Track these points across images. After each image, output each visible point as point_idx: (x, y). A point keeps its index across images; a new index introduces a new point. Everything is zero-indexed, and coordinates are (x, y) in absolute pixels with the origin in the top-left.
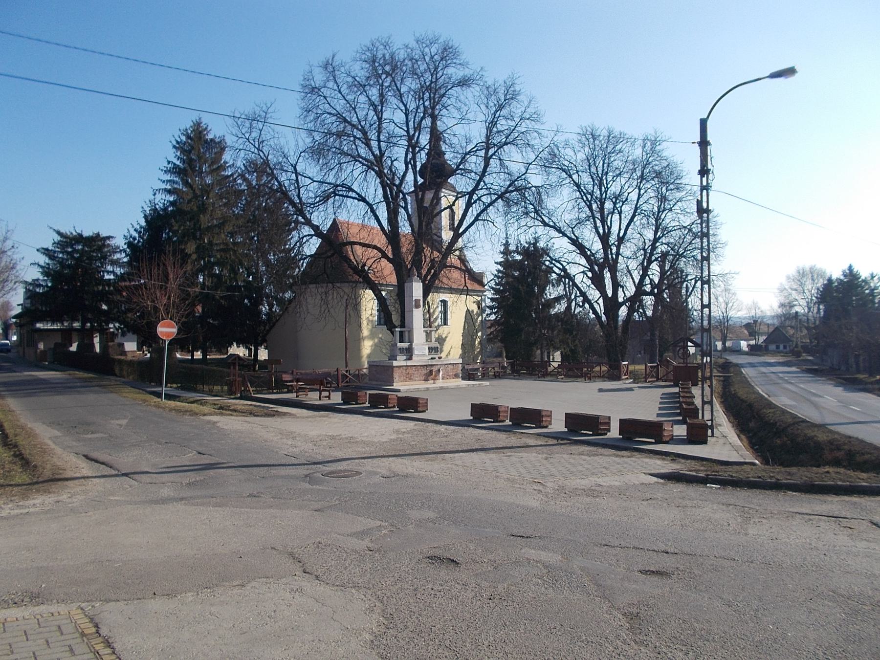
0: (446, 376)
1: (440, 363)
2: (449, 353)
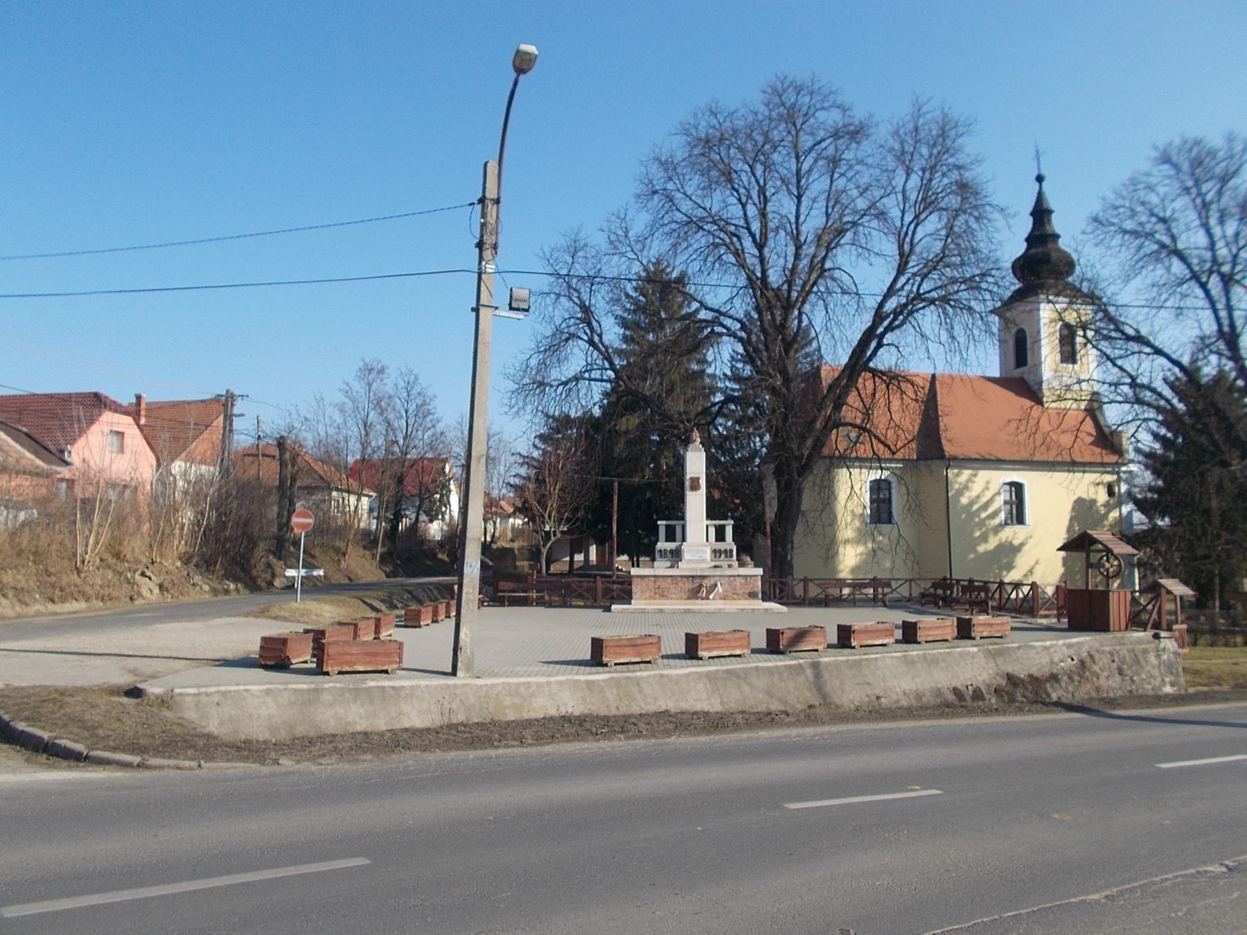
0: (730, 594)
1: (718, 573)
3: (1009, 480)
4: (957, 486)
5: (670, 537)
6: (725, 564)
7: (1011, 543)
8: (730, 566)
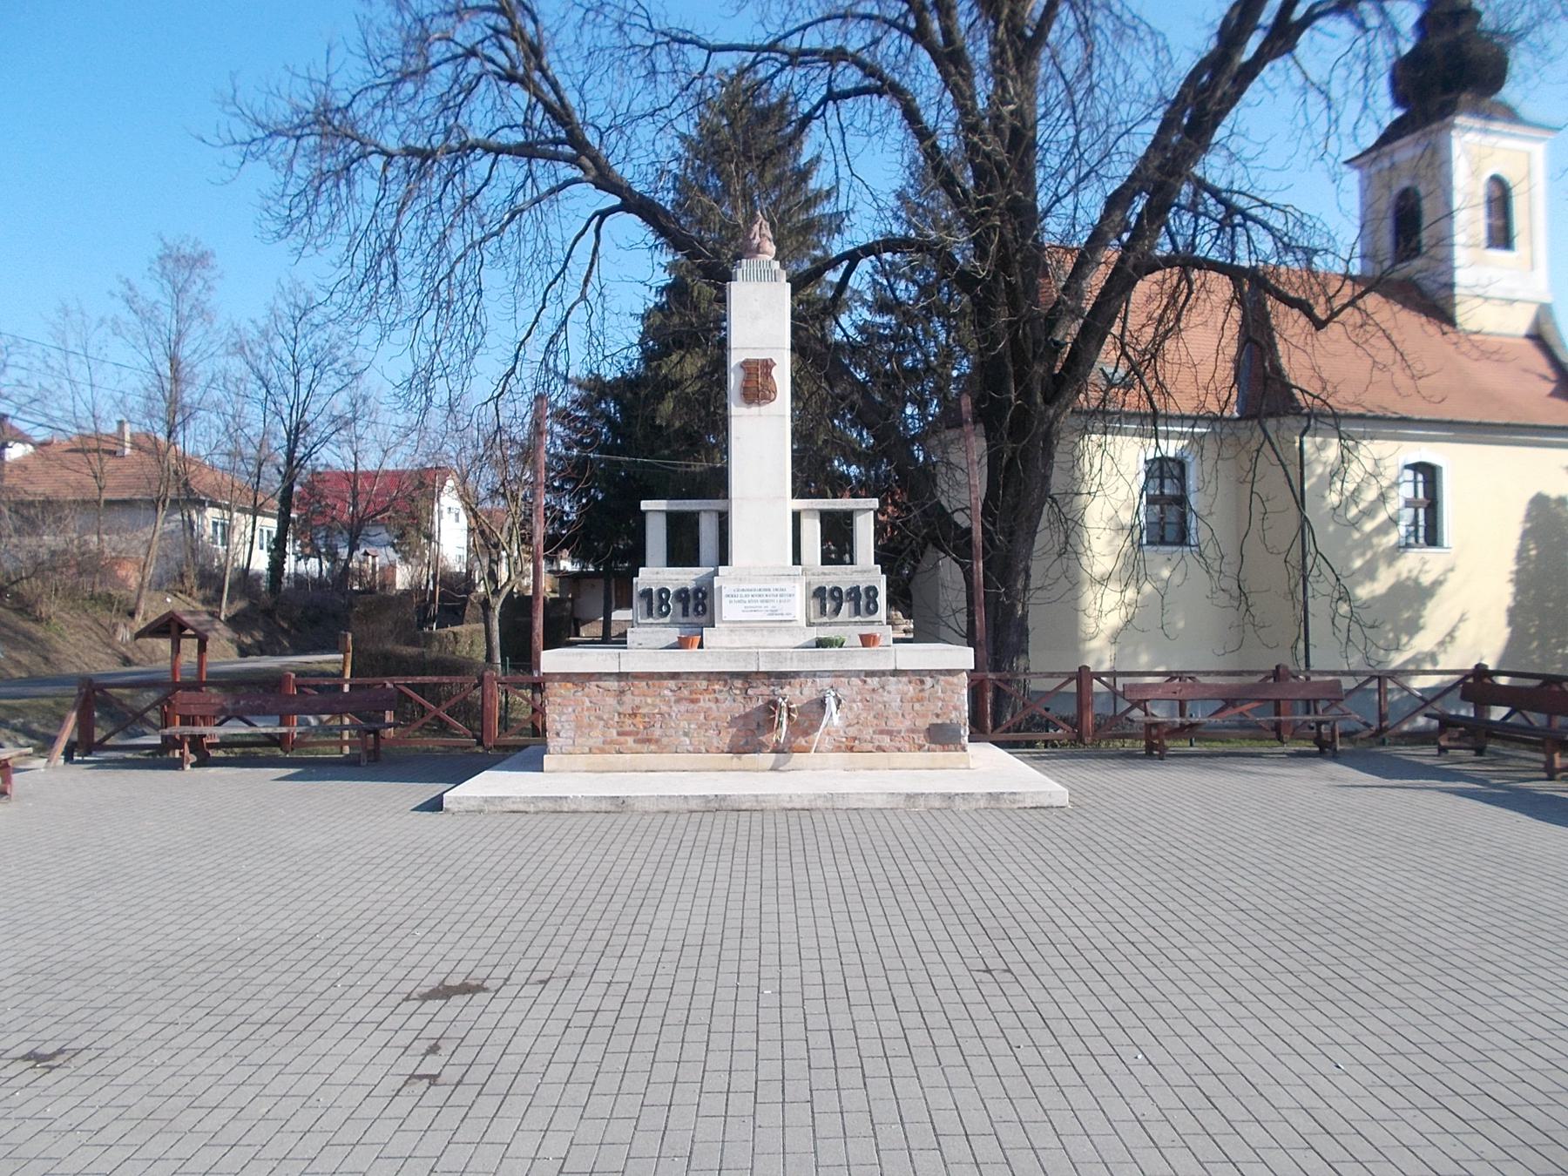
0: (868, 733)
2: (1451, 635)
3: (1414, 459)
4: (1319, 470)
5: (682, 550)
6: (851, 634)
7: (1416, 581)
8: (867, 641)
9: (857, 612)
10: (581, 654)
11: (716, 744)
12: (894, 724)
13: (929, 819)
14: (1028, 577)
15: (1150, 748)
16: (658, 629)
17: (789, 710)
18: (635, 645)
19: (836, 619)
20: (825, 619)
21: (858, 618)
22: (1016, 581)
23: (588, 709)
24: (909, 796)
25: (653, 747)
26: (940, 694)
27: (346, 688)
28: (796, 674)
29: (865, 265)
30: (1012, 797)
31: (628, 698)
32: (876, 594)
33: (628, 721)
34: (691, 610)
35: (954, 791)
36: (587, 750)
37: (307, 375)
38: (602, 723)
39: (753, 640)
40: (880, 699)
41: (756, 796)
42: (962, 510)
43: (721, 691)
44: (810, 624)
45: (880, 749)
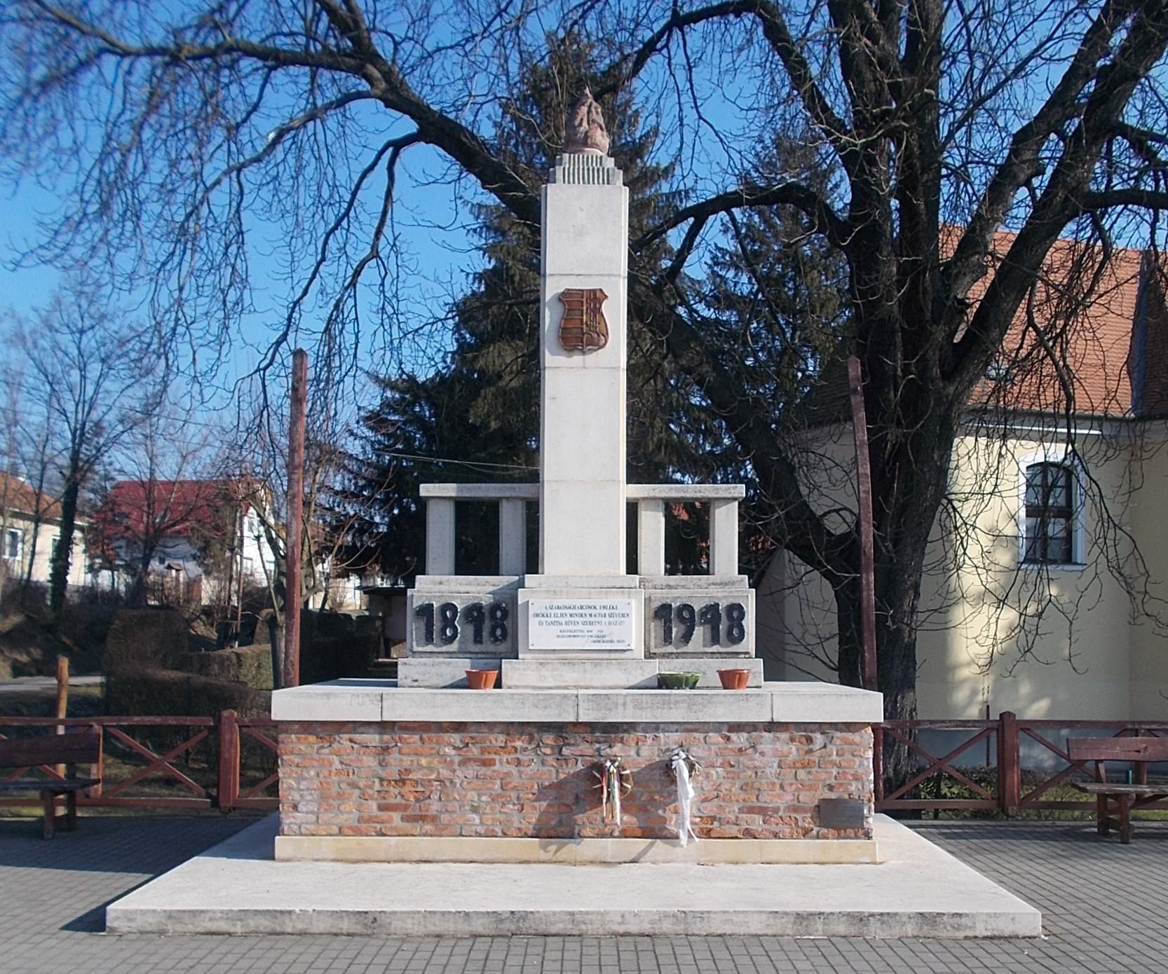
6: (709, 669)
8: (730, 680)
9: (715, 640)
10: (328, 695)
11: (516, 824)
12: (768, 799)
13: (829, 950)
14: (917, 595)
15: (1104, 824)
16: (441, 660)
17: (621, 778)
18: (409, 682)
19: (684, 649)
20: (670, 649)
21: (715, 648)
22: (901, 600)
23: (338, 772)
24: (800, 917)
25: (428, 827)
26: (834, 757)
27: (61, 730)
28: (631, 727)
29: (715, 222)
30: (957, 920)
31: (393, 757)
32: (742, 614)
33: (394, 791)
34: (485, 634)
35: (867, 910)
36: (335, 829)
37: (95, 369)
38: (357, 792)
39: (570, 676)
40: (750, 764)
41: (572, 914)
42: (837, 511)
43: (525, 749)
44: (649, 655)
45: (749, 834)
